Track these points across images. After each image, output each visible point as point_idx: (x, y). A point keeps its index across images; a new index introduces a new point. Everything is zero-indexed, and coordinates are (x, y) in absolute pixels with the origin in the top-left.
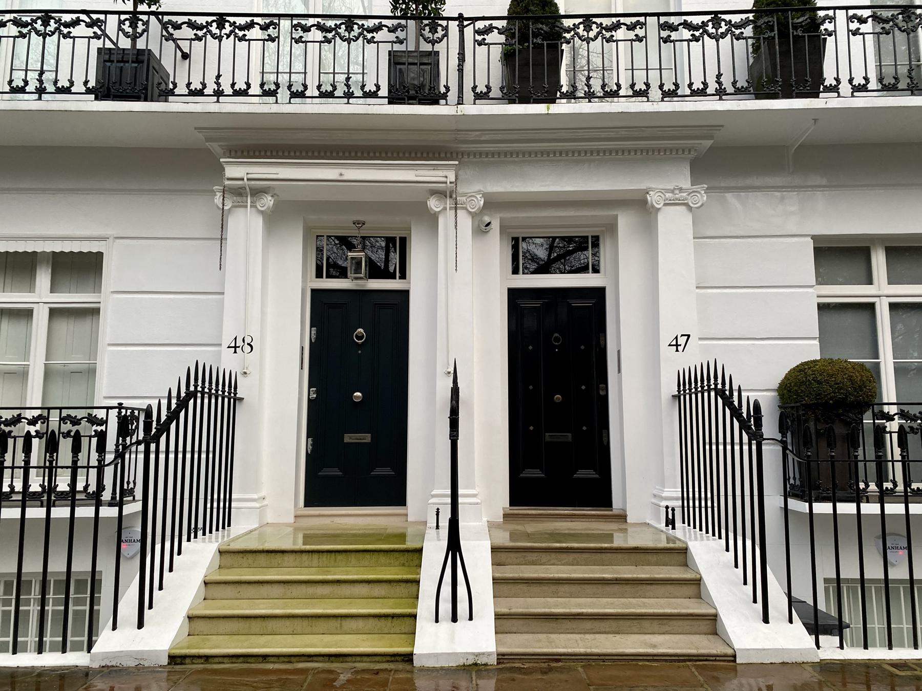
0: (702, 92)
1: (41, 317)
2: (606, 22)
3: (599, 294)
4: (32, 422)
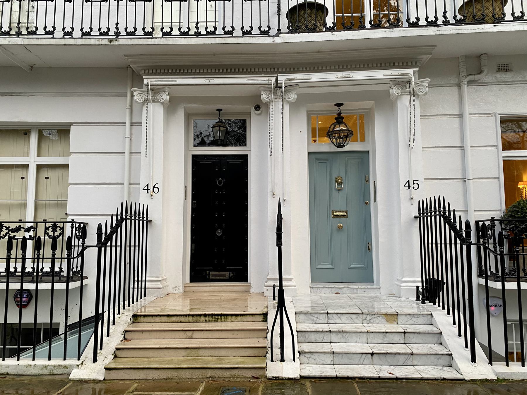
0: (186, 34)
1: (32, 170)
4: (28, 230)
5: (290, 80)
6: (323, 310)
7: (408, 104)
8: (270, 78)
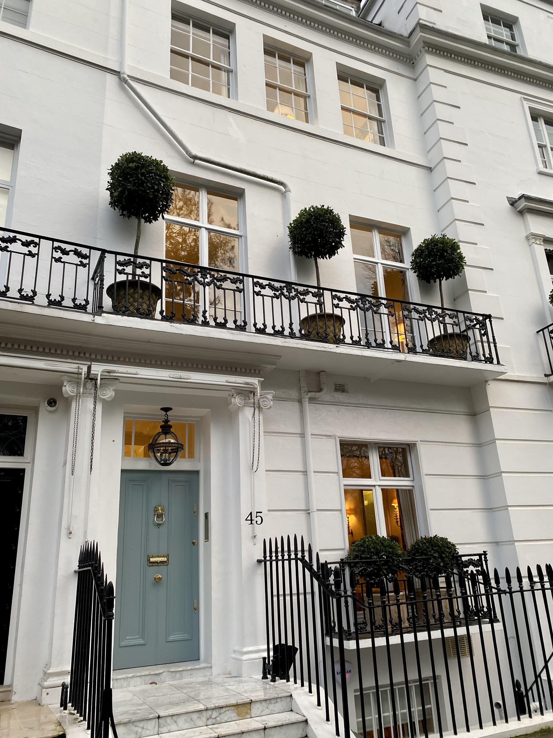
2: (301, 289)
5: (108, 372)
6: (151, 713)
7: (250, 417)
8: (81, 366)
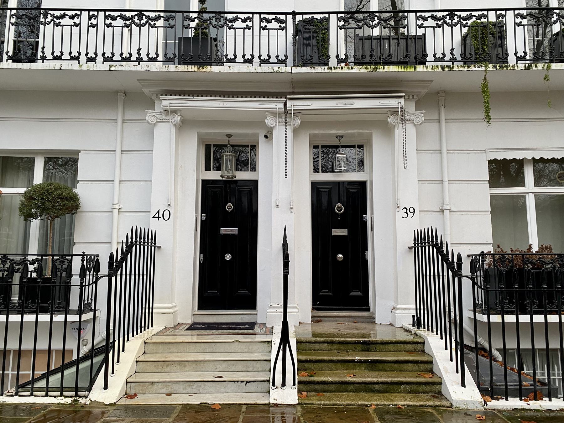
0: (128, 59)
2: (152, 15)
3: (362, 185)
